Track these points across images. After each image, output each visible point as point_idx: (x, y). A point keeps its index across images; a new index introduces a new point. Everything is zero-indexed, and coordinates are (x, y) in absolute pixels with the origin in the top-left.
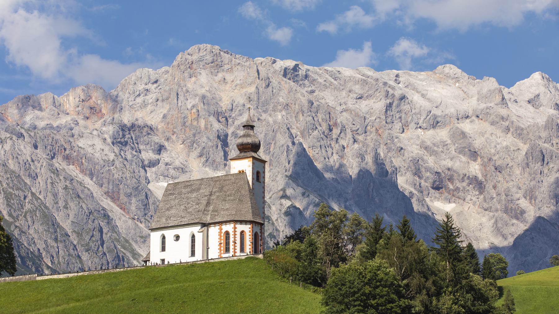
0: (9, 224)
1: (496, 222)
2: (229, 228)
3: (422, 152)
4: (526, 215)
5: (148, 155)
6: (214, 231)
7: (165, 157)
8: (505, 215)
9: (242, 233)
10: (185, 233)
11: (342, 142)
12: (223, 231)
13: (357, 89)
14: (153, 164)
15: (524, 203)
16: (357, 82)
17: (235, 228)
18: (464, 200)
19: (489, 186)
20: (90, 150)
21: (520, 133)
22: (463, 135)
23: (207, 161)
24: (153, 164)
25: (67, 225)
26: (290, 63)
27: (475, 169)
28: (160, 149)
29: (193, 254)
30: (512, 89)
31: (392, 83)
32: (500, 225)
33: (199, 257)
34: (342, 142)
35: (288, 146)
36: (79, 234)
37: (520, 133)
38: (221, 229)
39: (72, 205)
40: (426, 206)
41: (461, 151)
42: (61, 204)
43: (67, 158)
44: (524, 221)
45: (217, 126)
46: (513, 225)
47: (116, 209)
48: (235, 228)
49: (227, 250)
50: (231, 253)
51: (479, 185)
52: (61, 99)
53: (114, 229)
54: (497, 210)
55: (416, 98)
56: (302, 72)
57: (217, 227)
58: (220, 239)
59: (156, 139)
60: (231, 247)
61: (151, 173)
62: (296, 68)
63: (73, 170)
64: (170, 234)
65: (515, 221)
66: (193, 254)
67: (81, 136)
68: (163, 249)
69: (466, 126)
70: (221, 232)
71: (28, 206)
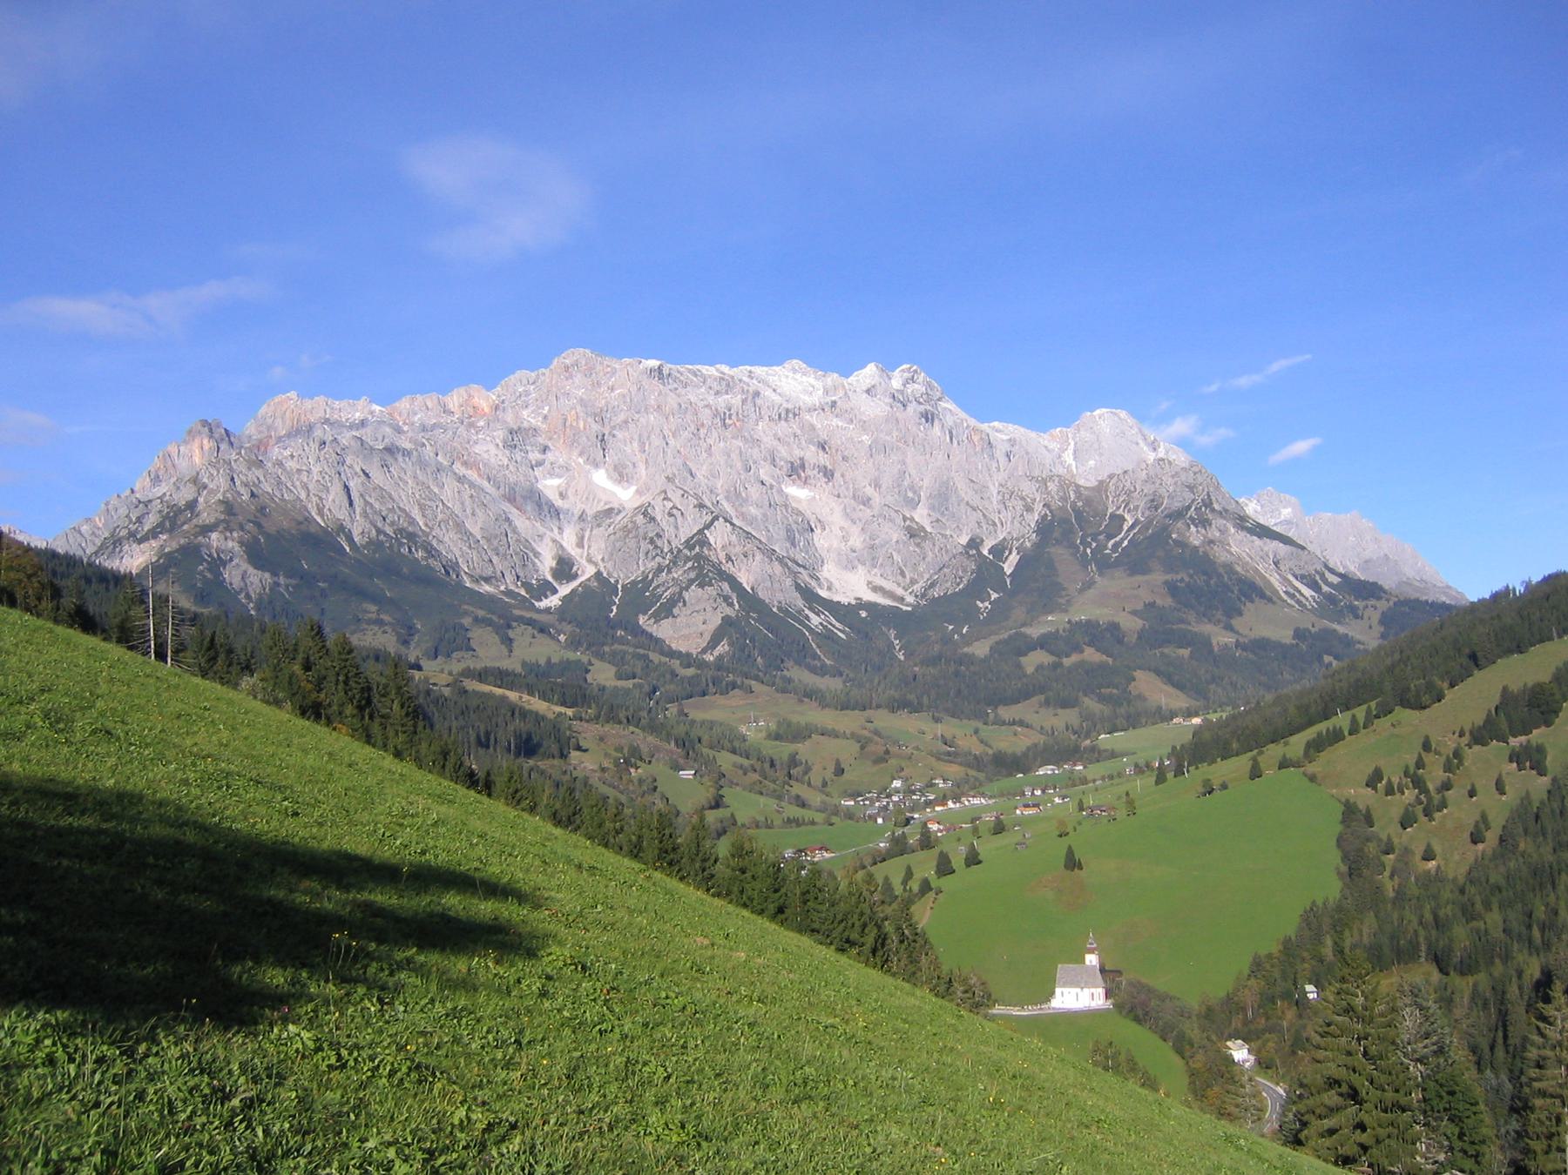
0: (427, 535)
3: (776, 443)
5: (535, 456)
7: (550, 456)
11: (710, 441)
13: (716, 386)
14: (540, 464)
15: (869, 491)
21: (864, 426)
22: (813, 428)
24: (540, 464)
25: (476, 531)
26: (654, 363)
27: (823, 459)
28: (545, 449)
30: (851, 379)
31: (745, 379)
34: (710, 441)
36: (488, 540)
37: (864, 426)
39: (479, 513)
40: (1511, 1049)
41: (810, 442)
42: (469, 511)
43: (465, 464)
44: (870, 507)
45: (595, 427)
47: (514, 510)
51: (828, 474)
52: (447, 399)
53: (515, 531)
55: (768, 393)
56: (666, 372)
59: (541, 440)
61: (538, 472)
62: (660, 368)
63: (472, 475)
67: (476, 443)
69: (812, 419)
71: (440, 517)
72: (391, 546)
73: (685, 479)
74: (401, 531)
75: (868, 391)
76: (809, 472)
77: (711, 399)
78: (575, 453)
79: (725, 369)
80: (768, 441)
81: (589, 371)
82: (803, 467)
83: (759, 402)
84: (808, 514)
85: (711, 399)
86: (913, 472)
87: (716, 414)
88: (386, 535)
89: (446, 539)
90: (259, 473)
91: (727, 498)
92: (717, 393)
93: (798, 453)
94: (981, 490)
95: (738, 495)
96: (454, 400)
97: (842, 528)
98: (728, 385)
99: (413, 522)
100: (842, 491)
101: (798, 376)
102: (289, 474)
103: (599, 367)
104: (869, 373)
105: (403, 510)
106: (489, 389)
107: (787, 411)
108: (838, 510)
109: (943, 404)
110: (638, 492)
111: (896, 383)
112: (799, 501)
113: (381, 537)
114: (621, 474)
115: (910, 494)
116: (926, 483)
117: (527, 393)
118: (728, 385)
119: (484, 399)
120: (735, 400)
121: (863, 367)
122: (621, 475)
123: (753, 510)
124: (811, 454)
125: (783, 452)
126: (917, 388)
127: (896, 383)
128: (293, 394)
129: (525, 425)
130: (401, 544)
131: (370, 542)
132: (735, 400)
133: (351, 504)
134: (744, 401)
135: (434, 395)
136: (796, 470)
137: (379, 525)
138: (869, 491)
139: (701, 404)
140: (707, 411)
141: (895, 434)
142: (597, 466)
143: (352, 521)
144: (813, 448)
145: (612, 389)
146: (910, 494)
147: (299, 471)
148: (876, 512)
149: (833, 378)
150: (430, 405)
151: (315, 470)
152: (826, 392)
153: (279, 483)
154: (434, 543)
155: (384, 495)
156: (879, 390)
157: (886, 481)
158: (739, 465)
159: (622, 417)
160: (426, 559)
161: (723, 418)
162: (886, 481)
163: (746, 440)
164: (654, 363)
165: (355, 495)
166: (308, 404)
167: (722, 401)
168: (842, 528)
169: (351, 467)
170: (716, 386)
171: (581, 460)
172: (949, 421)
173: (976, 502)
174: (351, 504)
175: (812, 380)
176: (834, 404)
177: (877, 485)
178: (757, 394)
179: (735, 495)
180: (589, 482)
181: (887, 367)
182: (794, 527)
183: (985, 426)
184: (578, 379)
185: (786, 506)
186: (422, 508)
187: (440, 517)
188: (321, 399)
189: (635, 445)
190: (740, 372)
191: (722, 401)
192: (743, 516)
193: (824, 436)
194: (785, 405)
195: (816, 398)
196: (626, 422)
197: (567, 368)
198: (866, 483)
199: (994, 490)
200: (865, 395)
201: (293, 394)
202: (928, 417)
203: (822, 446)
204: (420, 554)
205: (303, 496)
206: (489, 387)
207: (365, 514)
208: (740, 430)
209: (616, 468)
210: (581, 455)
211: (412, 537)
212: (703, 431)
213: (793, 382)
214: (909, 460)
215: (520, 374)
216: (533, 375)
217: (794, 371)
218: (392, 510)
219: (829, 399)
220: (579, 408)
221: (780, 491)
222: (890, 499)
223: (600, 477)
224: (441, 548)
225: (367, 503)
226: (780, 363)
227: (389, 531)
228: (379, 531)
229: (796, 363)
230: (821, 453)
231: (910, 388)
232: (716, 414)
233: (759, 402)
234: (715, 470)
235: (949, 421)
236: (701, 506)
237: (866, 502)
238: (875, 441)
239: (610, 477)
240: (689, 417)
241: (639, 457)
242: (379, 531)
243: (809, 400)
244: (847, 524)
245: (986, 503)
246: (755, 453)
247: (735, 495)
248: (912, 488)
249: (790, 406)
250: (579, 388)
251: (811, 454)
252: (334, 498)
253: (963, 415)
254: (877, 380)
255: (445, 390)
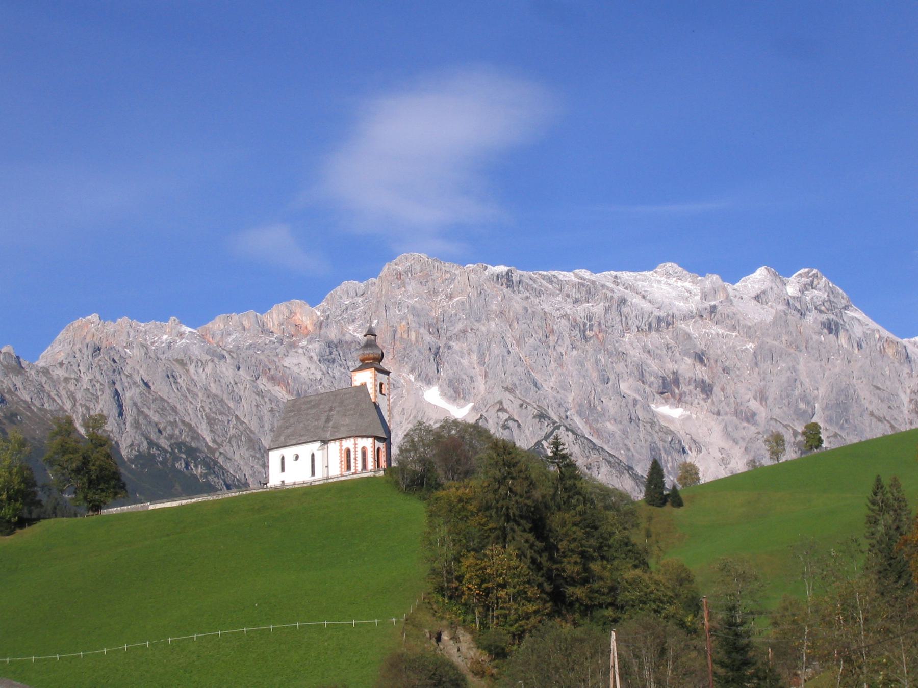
0: (212, 451)
1: (726, 427)
2: (348, 443)
3: (645, 356)
4: (757, 418)
6: (334, 447)
8: (735, 418)
9: (379, 449)
10: (305, 450)
12: (344, 448)
13: (574, 294)
15: (754, 405)
16: (574, 286)
17: (355, 444)
18: (691, 404)
19: (716, 389)
20: (296, 369)
21: (749, 332)
22: (688, 336)
23: (419, 375)
26: (502, 269)
27: (701, 372)
29: (313, 474)
31: (610, 285)
32: (730, 429)
33: (319, 475)
34: (562, 350)
35: (503, 356)
37: (749, 332)
38: (341, 446)
41: (686, 353)
43: (272, 379)
44: (755, 424)
45: (429, 338)
46: (744, 428)
48: (355, 444)
49: (349, 468)
50: (353, 470)
51: (706, 389)
54: (726, 414)
55: (636, 300)
56: (515, 278)
57: (338, 443)
58: (341, 456)
60: (352, 464)
62: (508, 275)
64: (289, 452)
65: (745, 424)
66: (313, 474)
68: (283, 470)
70: (341, 450)
72: (164, 463)
73: (527, 390)
74: (180, 445)
75: (757, 298)
76: (684, 388)
77: (568, 308)
78: (406, 369)
79: (586, 274)
80: (635, 354)
81: (425, 278)
82: (676, 382)
83: (625, 310)
84: (682, 435)
85: (568, 308)
86: (807, 381)
87: (575, 325)
88: (158, 447)
89: (237, 457)
90: (18, 380)
91: (580, 413)
92: (576, 301)
93: (670, 366)
94: (890, 399)
95: (592, 408)
96: (274, 317)
97: (721, 450)
98: (589, 292)
99: (196, 437)
100: (723, 407)
101: (672, 281)
102: (55, 383)
103: (436, 274)
104: (760, 277)
105: (189, 426)
106: (313, 305)
107: (659, 320)
108: (717, 429)
109: (850, 313)
110: (474, 409)
111: (792, 290)
112: (671, 420)
113: (154, 450)
114: (456, 392)
115: (802, 406)
116: (822, 392)
117: (354, 306)
118: (589, 292)
119: (306, 315)
120: (597, 309)
121: (753, 271)
122: (456, 392)
123: (610, 426)
124: (686, 367)
125: (653, 365)
126: (818, 295)
127: (792, 290)
128: (94, 317)
129: (348, 338)
130: (177, 459)
131: (140, 456)
132: (597, 309)
133: (121, 414)
134: (607, 310)
135: (252, 313)
136: (669, 387)
137: (153, 437)
138: (754, 405)
139: (557, 314)
140: (564, 321)
141: (785, 338)
142: (429, 382)
143: (121, 432)
144: (689, 361)
145: (450, 297)
146: (802, 406)
147: (67, 380)
148: (761, 429)
149: (713, 280)
150: (246, 323)
151: (85, 378)
152: (705, 296)
153: (41, 389)
154: (221, 460)
155: (164, 407)
156: (771, 296)
157: (773, 392)
158: (595, 374)
159: (460, 326)
160: (206, 476)
161: (583, 330)
162: (773, 392)
163: (610, 354)
164: (502, 269)
165: (127, 403)
166: (110, 327)
167: (581, 310)
168: (721, 450)
169: (130, 376)
170: (574, 294)
171: (412, 377)
172: (858, 331)
173: (882, 411)
174: (121, 414)
175: (688, 285)
176: (713, 309)
177: (762, 397)
178: (623, 301)
179: (589, 410)
180: (420, 400)
181: (783, 270)
182: (660, 444)
183: (905, 341)
184: (412, 287)
185: (653, 424)
186: (211, 422)
187: (232, 432)
188: (124, 321)
189: (474, 357)
190: (605, 277)
191: (581, 310)
192: (597, 432)
193: (701, 345)
194: (657, 313)
195: (694, 304)
196: (464, 332)
197: (399, 275)
198: (750, 395)
199: (905, 398)
200: (754, 302)
201: (94, 317)
202: (832, 328)
203: (700, 358)
204: (199, 471)
205: (68, 406)
206: (314, 302)
207: (137, 425)
208: (603, 343)
209: (450, 383)
210: (412, 370)
211: (192, 453)
212: (552, 339)
213: (667, 287)
214: (801, 367)
215: (345, 285)
216: (362, 285)
217: (668, 275)
218: (174, 424)
219: (707, 304)
220: (410, 317)
221: (647, 408)
222: (777, 412)
223: (433, 395)
224: (228, 466)
225: (140, 412)
226: (651, 267)
227: (164, 443)
228: (151, 444)
229: (670, 266)
230: (698, 366)
231: (809, 295)
232: (575, 325)
233: (625, 310)
234: (564, 383)
235: (858, 331)
236: (542, 416)
237: (751, 417)
238: (760, 347)
239: (444, 394)
240: (536, 322)
241: (478, 370)
242: (151, 444)
243: (682, 306)
244: (727, 445)
245: (895, 413)
246: (620, 367)
247: (589, 410)
248: (804, 398)
249: (662, 314)
250: (411, 297)
251: (686, 367)
252: (104, 405)
253: (873, 325)
254: (767, 284)
255: (263, 306)
